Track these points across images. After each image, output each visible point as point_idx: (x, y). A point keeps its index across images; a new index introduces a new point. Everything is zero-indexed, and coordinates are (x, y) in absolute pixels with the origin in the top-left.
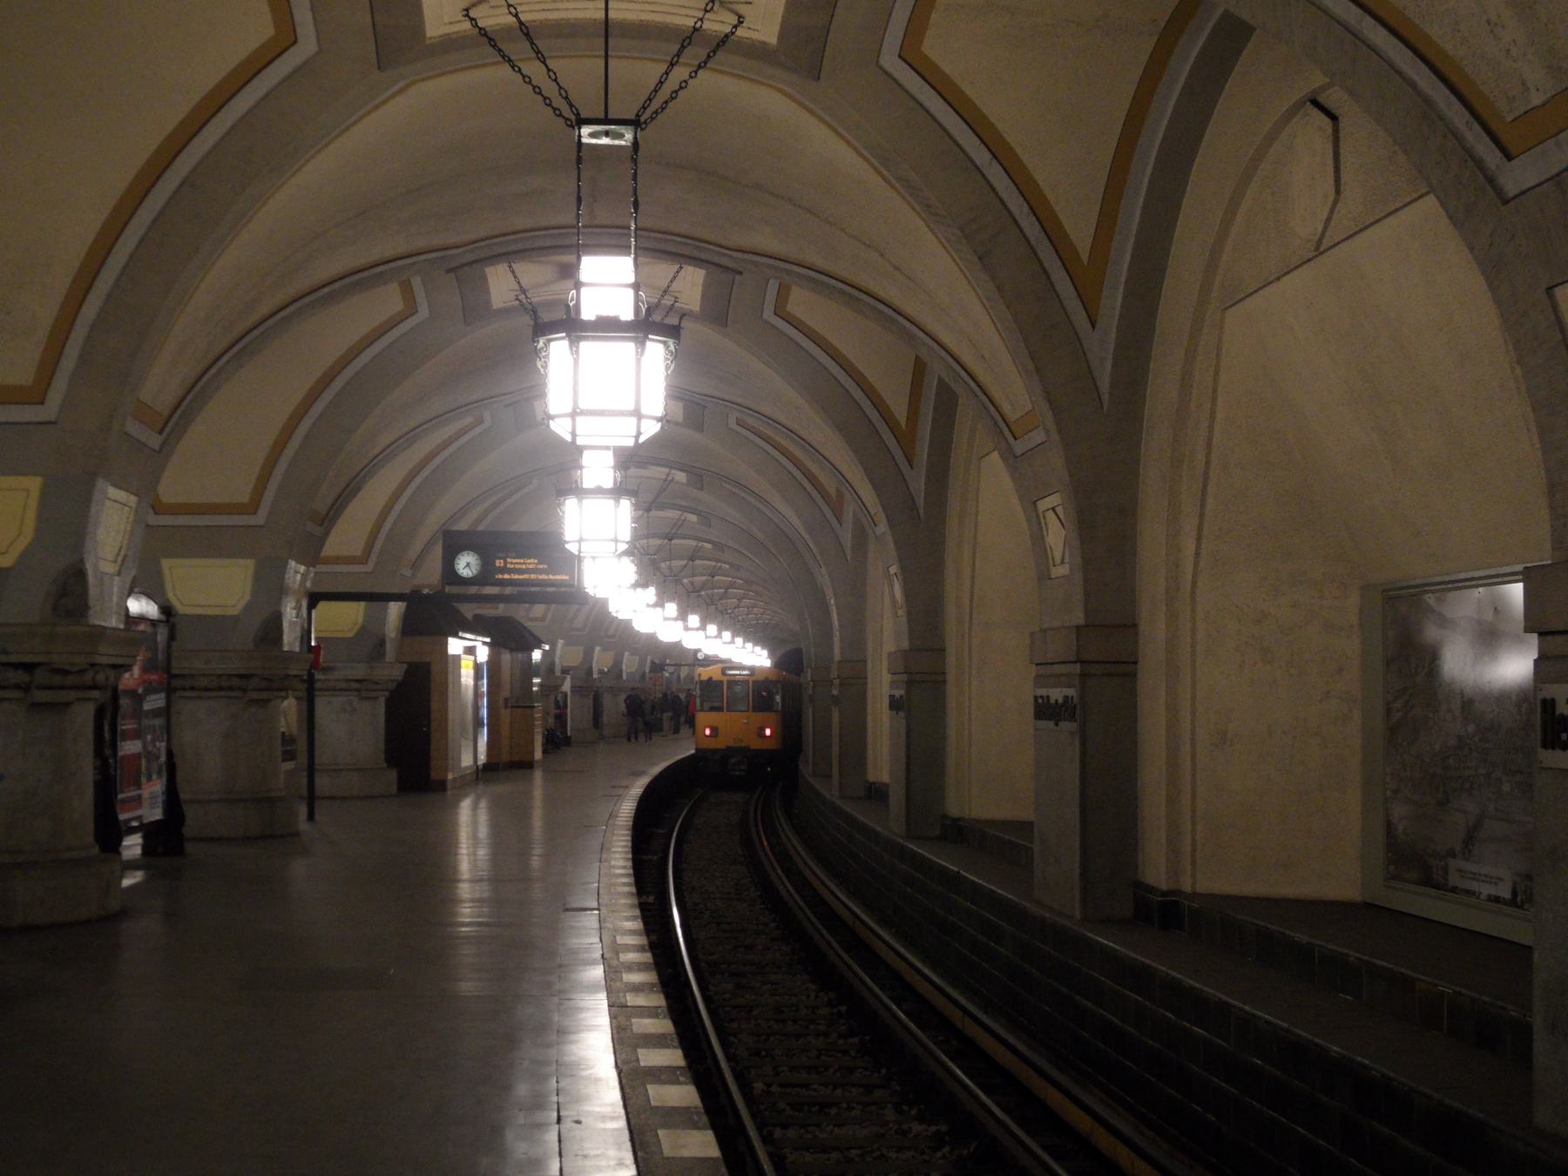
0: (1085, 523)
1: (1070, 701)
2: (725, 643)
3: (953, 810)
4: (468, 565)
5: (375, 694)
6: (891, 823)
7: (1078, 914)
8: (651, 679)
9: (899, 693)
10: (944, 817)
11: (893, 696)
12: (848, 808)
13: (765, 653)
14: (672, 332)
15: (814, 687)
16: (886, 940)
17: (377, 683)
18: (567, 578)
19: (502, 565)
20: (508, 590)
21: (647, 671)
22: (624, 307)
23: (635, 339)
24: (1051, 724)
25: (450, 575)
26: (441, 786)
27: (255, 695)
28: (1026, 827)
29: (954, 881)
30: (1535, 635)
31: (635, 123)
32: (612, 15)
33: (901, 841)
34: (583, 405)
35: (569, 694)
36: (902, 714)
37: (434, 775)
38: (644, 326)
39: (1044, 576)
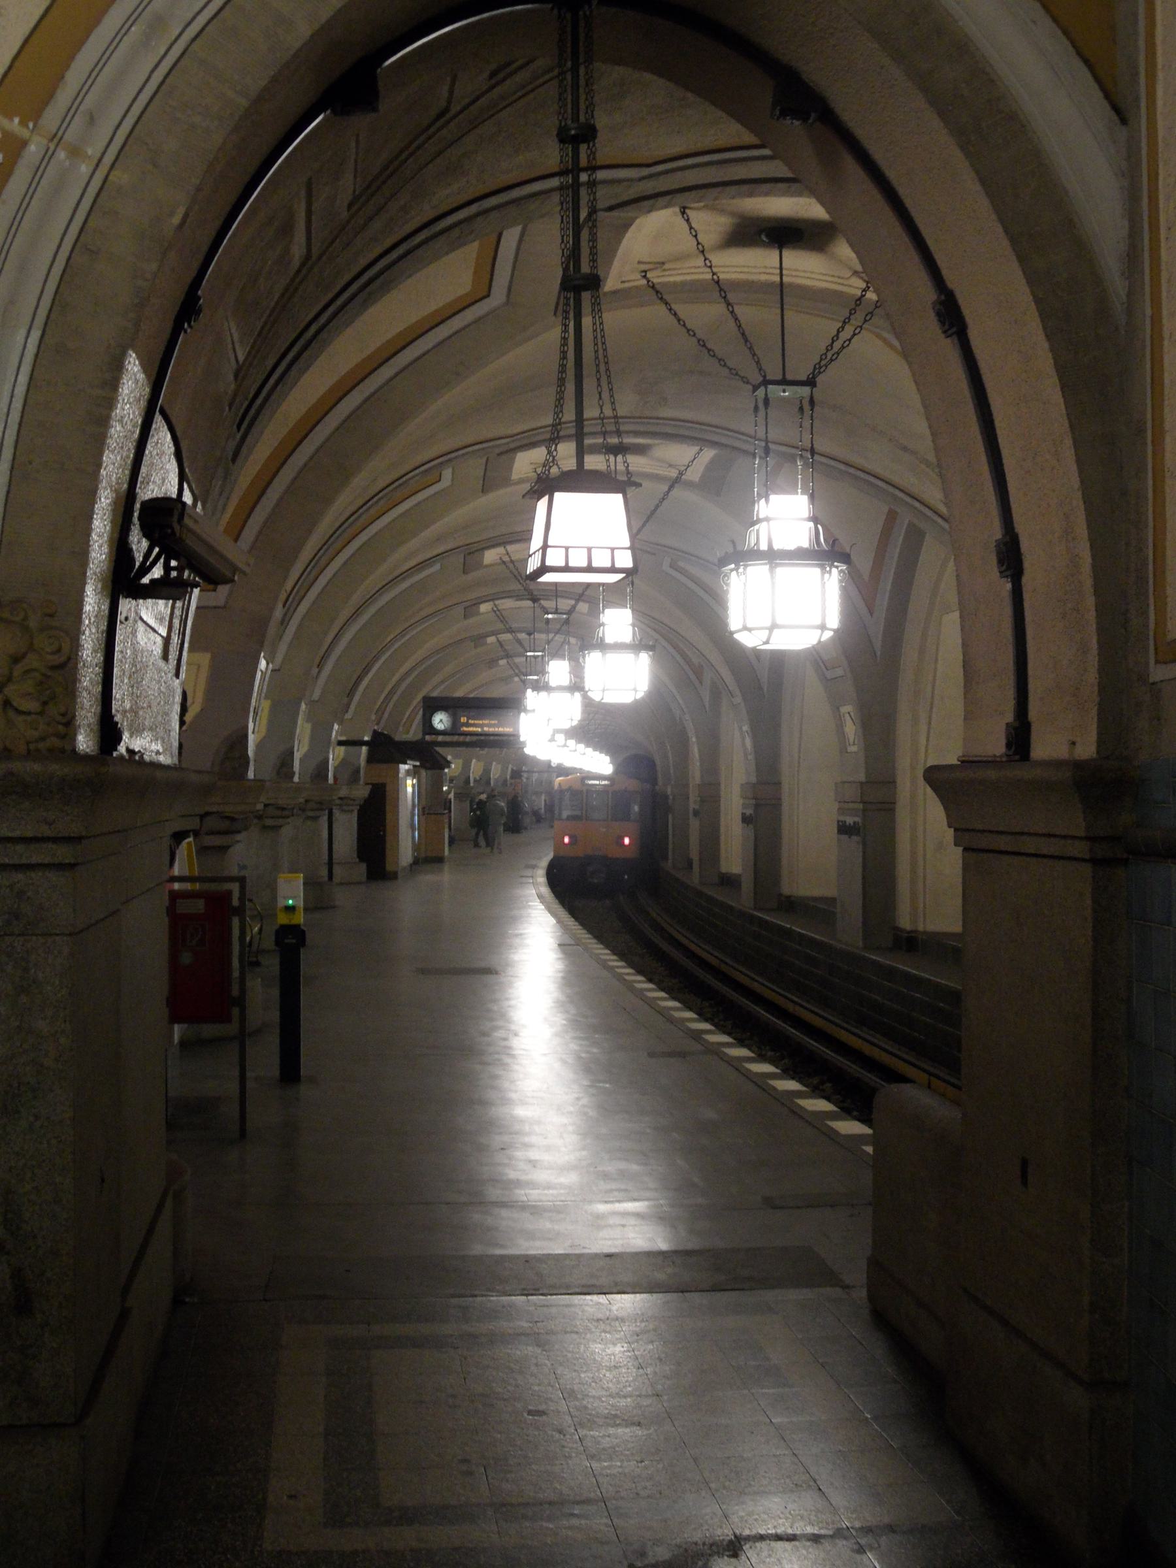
0: (866, 724)
2: (559, 746)
3: (786, 890)
4: (441, 721)
5: (351, 808)
6: (745, 900)
7: (861, 944)
8: (511, 784)
9: (749, 812)
10: (780, 895)
11: (745, 814)
12: (710, 892)
13: (607, 759)
14: (845, 558)
15: (674, 799)
16: (743, 975)
17: (354, 800)
18: (511, 730)
19: (463, 720)
20: (468, 739)
21: (508, 777)
24: (847, 836)
25: (429, 728)
26: (394, 876)
27: (310, 814)
28: (832, 901)
29: (788, 933)
30: (953, 829)
31: (811, 382)
32: (785, 279)
33: (751, 911)
35: (452, 800)
36: (751, 826)
37: (389, 867)
39: (843, 750)
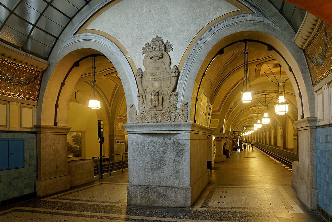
22: (283, 101)
38: (285, 103)
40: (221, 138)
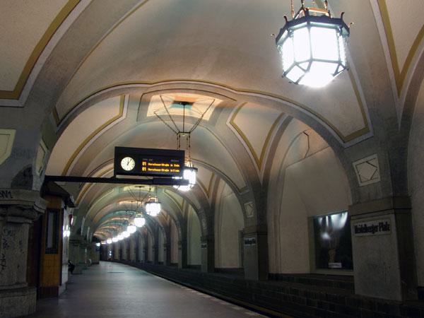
1: (384, 224)
19: (144, 163)
23: (336, 28)
34: (314, 58)
40: (18, 212)
